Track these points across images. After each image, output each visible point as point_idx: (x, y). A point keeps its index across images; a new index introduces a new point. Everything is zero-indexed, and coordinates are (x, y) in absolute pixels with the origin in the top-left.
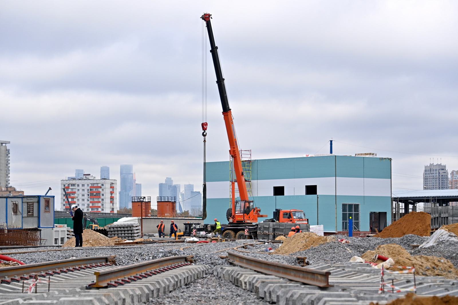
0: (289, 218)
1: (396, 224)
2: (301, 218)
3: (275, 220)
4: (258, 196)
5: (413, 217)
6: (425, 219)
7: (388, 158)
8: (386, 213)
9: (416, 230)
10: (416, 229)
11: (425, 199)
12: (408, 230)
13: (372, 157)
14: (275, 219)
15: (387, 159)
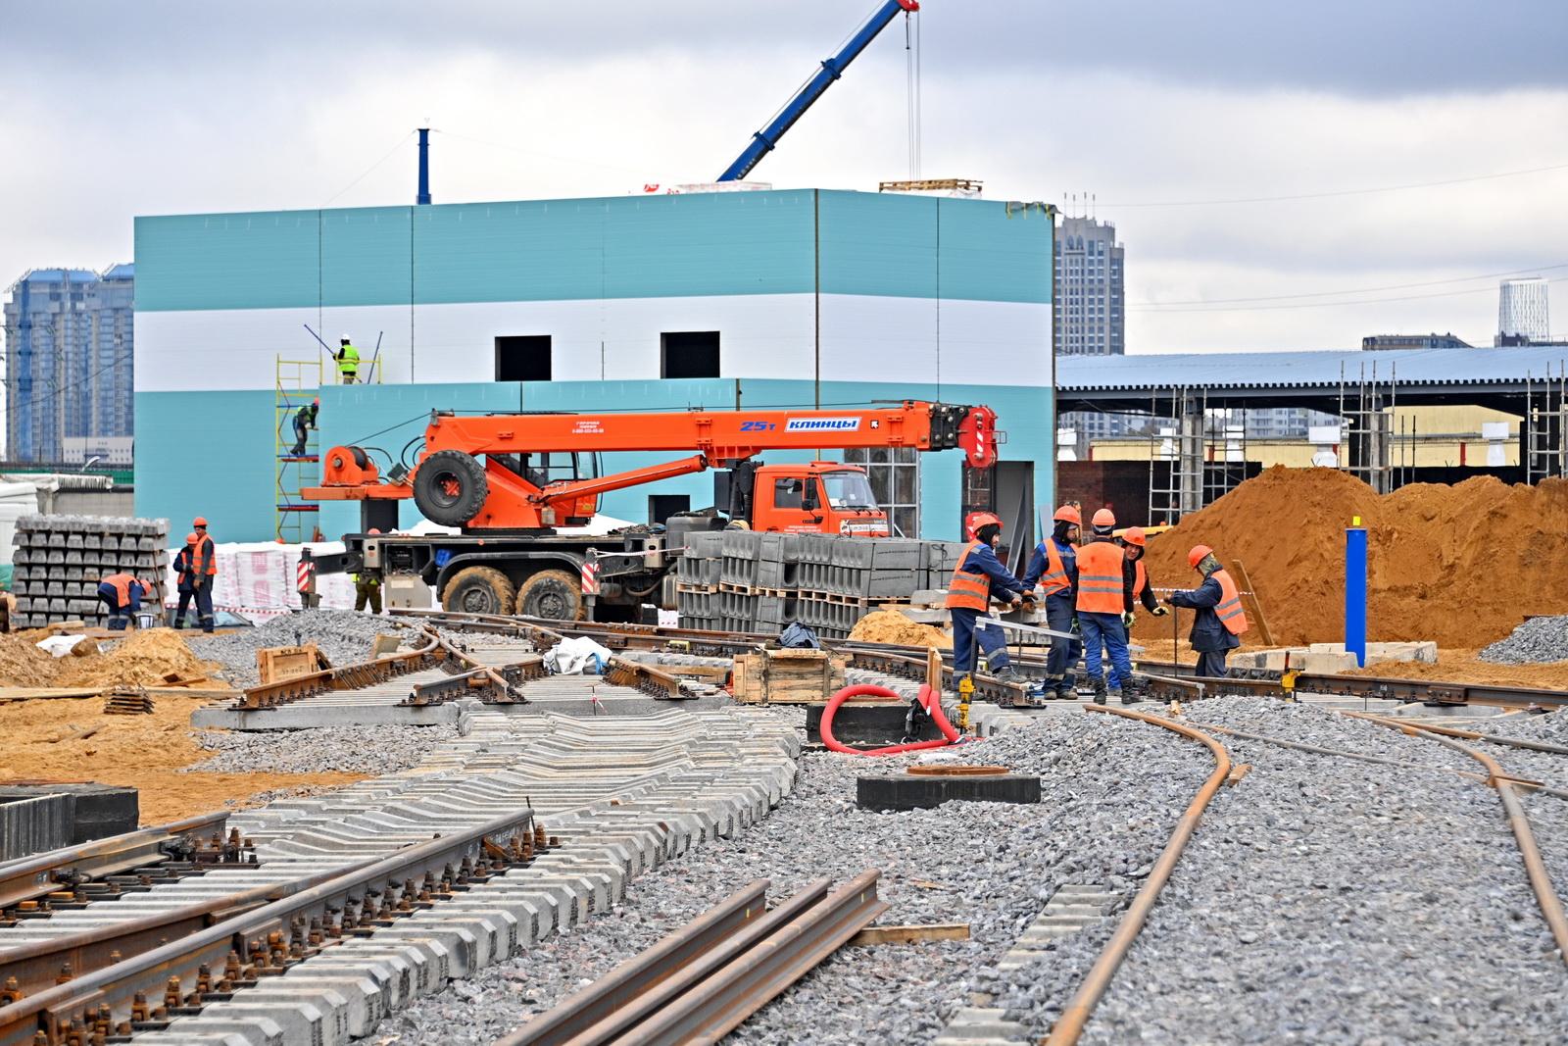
0: (807, 507)
1: (1198, 527)
2: (864, 508)
3: (727, 516)
4: (416, 382)
5: (1287, 496)
6: (1347, 502)
7: (1042, 206)
8: (1029, 465)
9: (1306, 558)
10: (1306, 551)
11: (1154, 396)
12: (1265, 558)
13: (963, 197)
14: (727, 512)
15: (1039, 211)
